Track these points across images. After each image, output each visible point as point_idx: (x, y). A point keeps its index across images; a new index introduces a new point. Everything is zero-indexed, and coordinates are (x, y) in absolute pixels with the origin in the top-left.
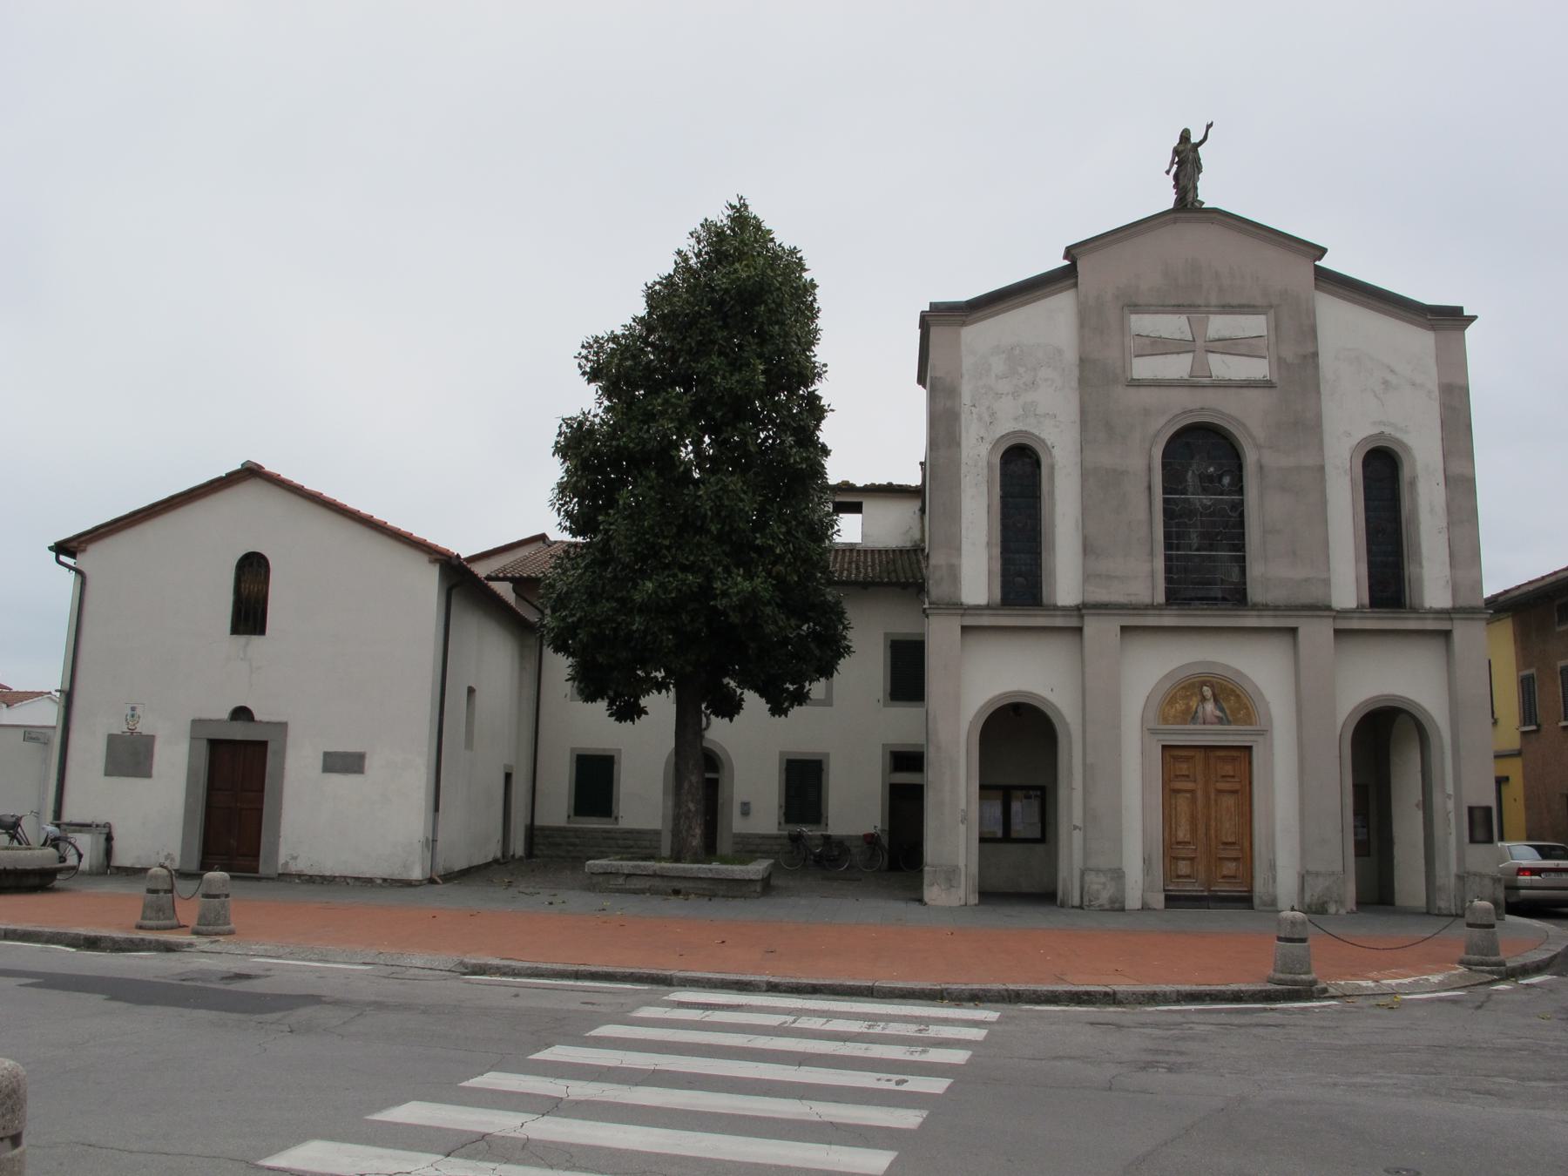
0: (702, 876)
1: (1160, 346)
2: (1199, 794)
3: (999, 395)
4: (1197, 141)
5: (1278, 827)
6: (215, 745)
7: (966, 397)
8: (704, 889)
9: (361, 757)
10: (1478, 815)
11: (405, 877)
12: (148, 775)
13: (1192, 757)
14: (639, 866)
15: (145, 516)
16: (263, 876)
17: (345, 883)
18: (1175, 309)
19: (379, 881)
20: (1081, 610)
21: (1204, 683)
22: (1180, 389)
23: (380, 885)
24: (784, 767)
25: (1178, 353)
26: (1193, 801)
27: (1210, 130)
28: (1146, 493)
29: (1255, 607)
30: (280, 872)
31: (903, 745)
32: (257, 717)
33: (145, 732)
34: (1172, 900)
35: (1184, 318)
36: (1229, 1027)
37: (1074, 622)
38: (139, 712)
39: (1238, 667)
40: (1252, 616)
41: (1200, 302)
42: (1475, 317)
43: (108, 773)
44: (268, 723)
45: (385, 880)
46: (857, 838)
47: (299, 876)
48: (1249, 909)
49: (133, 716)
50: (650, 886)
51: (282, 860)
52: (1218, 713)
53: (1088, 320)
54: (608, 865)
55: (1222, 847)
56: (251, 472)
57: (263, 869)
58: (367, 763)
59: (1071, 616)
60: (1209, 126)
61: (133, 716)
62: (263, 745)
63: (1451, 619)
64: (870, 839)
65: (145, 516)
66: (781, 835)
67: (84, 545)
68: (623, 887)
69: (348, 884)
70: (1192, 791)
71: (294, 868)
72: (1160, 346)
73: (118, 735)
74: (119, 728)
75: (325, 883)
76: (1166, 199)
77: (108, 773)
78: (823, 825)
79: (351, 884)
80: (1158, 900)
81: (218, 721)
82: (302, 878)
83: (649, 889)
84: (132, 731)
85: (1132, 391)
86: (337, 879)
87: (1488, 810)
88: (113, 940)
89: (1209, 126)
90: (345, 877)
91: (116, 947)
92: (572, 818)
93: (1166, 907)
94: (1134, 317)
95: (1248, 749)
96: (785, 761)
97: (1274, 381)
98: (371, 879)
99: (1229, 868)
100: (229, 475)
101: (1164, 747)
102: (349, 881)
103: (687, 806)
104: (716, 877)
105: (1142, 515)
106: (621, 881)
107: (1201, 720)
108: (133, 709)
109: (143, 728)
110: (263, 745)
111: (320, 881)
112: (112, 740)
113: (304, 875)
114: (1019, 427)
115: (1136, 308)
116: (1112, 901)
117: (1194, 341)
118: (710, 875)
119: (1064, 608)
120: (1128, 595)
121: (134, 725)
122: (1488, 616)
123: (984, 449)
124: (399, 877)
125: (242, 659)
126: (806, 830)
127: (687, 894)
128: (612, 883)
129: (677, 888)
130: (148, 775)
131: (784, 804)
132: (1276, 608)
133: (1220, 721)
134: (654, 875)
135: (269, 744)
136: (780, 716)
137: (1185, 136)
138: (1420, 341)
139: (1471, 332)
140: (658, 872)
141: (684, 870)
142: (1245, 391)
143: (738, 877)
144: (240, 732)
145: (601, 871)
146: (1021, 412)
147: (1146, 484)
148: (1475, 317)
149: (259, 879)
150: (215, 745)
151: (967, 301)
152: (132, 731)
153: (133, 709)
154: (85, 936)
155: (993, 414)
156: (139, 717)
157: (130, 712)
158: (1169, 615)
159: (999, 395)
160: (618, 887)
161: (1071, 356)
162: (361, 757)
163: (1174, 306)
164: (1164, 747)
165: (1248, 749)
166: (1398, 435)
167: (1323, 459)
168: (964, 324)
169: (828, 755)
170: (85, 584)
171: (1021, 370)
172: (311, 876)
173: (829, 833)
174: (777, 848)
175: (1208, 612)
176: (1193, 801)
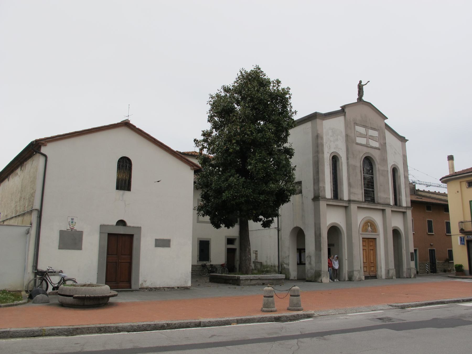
0: (271, 278)
1: (361, 135)
2: (367, 250)
3: (331, 141)
4: (363, 84)
5: (381, 258)
6: (110, 235)
7: (325, 141)
8: (271, 282)
9: (169, 241)
10: (412, 254)
11: (186, 286)
12: (80, 249)
13: (365, 241)
14: (255, 276)
15: (79, 134)
16: (134, 289)
17: (163, 290)
18: (363, 126)
19: (176, 288)
20: (349, 201)
21: (368, 222)
22: (361, 146)
23: (177, 290)
24: (199, 243)
25: (364, 138)
26: (366, 251)
27: (368, 83)
28: (360, 173)
29: (379, 203)
30: (140, 287)
31: (230, 236)
32: (128, 224)
33: (78, 229)
34: (366, 278)
35: (365, 129)
36: (450, 306)
37: (346, 205)
38: (75, 221)
39: (374, 218)
40: (379, 206)
41: (367, 126)
42: (408, 140)
43: (60, 248)
44: (133, 227)
45: (178, 287)
46: (219, 265)
47: (147, 288)
48: (376, 279)
49: (72, 222)
50: (257, 283)
51: (140, 283)
52: (371, 230)
53: (347, 125)
54: (247, 277)
55: (371, 263)
56: (126, 124)
57: (133, 287)
58: (171, 243)
59: (347, 203)
60: (369, 82)
61: (72, 222)
62: (131, 236)
63: (407, 209)
64: (222, 265)
65: (79, 134)
66: (198, 265)
67: (46, 143)
68: (250, 284)
69: (165, 290)
70: (366, 250)
71: (145, 285)
72: (361, 135)
73: (65, 231)
74: (65, 227)
75: (156, 290)
76: (354, 98)
77: (60, 248)
78: (209, 261)
79: (166, 290)
80: (363, 278)
81: (112, 225)
82: (148, 289)
83: (257, 284)
84: (72, 229)
85: (357, 145)
86: (161, 289)
87: (413, 253)
88: (286, 317)
89: (369, 82)
90: (164, 288)
91: (288, 319)
92: (199, 262)
93: (365, 279)
94: (356, 127)
95: (375, 239)
96: (199, 241)
97: (380, 148)
98: (173, 287)
99: (372, 269)
100: (118, 124)
101: (362, 238)
102: (165, 289)
103: (248, 256)
104: (275, 278)
105: (360, 178)
106: (249, 281)
107: (368, 231)
108: (72, 219)
109: (77, 228)
110: (131, 236)
111: (155, 290)
112: (62, 233)
113: (148, 288)
114: (335, 151)
115: (357, 124)
116: (359, 278)
117: (367, 135)
118: (273, 278)
119: (345, 201)
120: (358, 198)
121: (73, 226)
122: (412, 209)
123: (329, 155)
124: (183, 286)
125: (121, 200)
126: (205, 262)
127: (267, 284)
128: (246, 282)
129: (264, 283)
130: (80, 249)
131: (199, 255)
132: (383, 204)
133: (372, 232)
134: (259, 279)
135: (134, 235)
136: (214, 226)
137: (361, 82)
138: (399, 143)
139: (407, 143)
140: (260, 278)
141: (267, 277)
142: (375, 149)
143: (280, 278)
144: (121, 230)
145: (245, 279)
146: (335, 147)
147: (360, 171)
148: (408, 140)
149: (132, 291)
150: (110, 235)
151: (324, 114)
152: (72, 229)
153: (72, 219)
154: (274, 317)
155: (330, 146)
156: (75, 223)
157: (70, 220)
158: (366, 204)
159: (331, 141)
160: (248, 284)
161: (344, 134)
162: (169, 241)
163: (363, 125)
164: (362, 238)
165: (375, 239)
166: (397, 165)
167: (388, 169)
168: (324, 120)
169: (210, 239)
170: (45, 160)
171: (335, 135)
172: (151, 288)
173: (211, 264)
174: (197, 269)
175: (372, 204)
176: (366, 251)
